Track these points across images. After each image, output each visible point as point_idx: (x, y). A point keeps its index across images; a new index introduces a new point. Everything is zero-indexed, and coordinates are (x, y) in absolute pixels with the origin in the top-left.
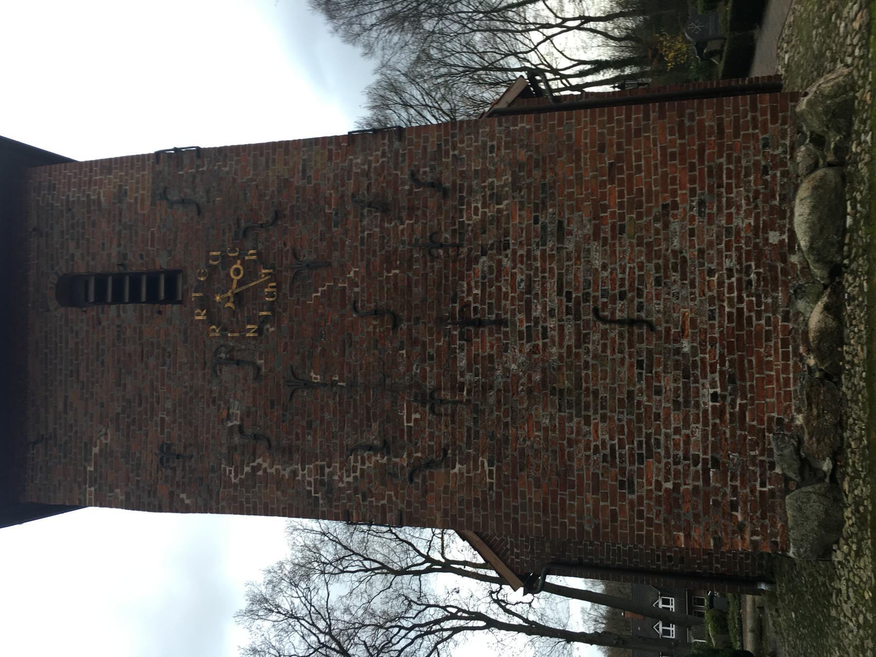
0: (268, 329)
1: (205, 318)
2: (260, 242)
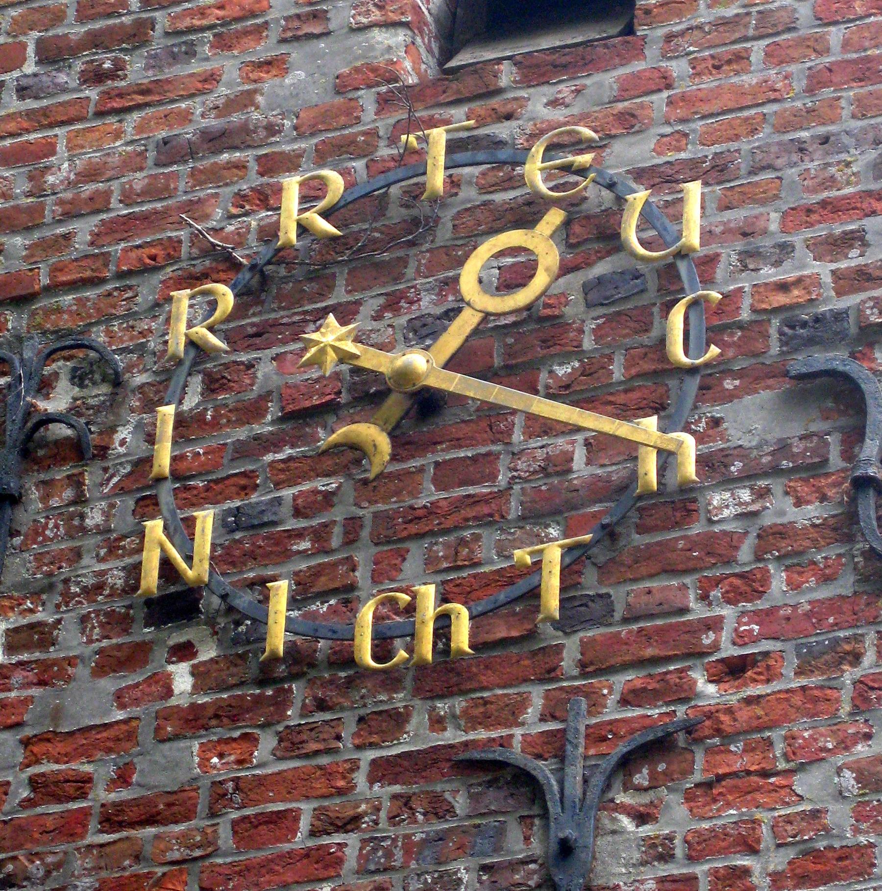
0: (184, 651)
1: (290, 233)
2: (761, 494)
